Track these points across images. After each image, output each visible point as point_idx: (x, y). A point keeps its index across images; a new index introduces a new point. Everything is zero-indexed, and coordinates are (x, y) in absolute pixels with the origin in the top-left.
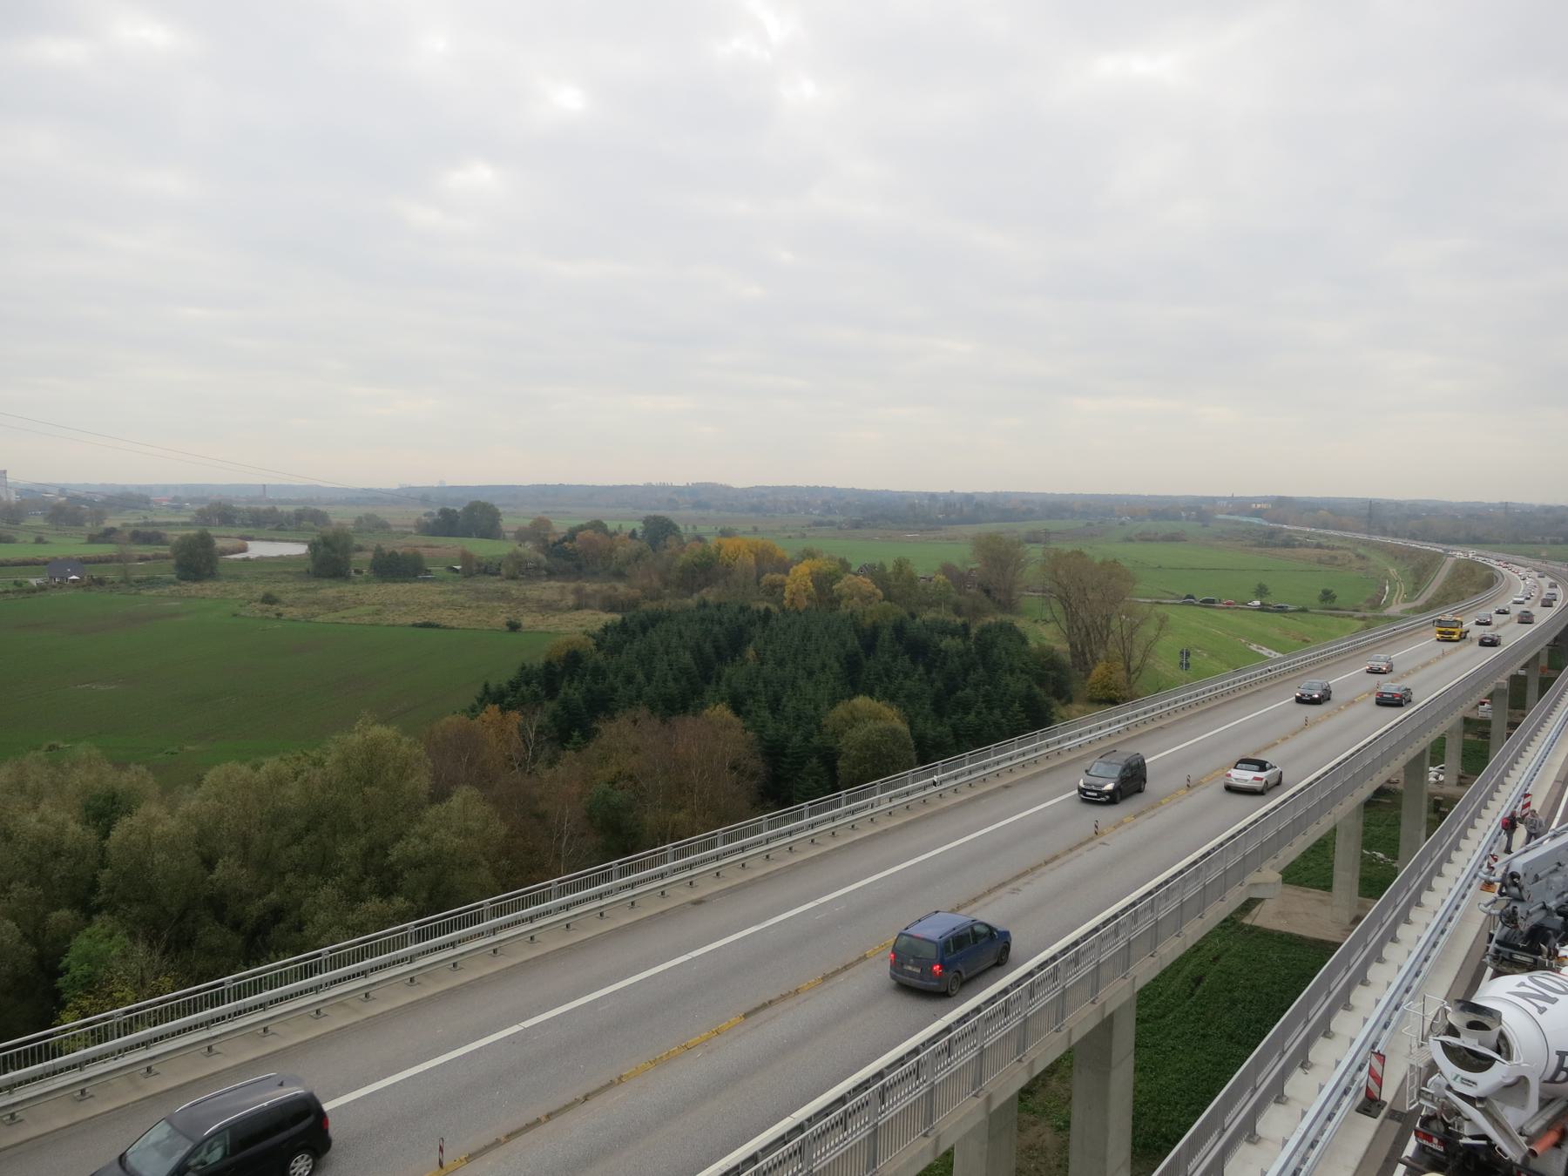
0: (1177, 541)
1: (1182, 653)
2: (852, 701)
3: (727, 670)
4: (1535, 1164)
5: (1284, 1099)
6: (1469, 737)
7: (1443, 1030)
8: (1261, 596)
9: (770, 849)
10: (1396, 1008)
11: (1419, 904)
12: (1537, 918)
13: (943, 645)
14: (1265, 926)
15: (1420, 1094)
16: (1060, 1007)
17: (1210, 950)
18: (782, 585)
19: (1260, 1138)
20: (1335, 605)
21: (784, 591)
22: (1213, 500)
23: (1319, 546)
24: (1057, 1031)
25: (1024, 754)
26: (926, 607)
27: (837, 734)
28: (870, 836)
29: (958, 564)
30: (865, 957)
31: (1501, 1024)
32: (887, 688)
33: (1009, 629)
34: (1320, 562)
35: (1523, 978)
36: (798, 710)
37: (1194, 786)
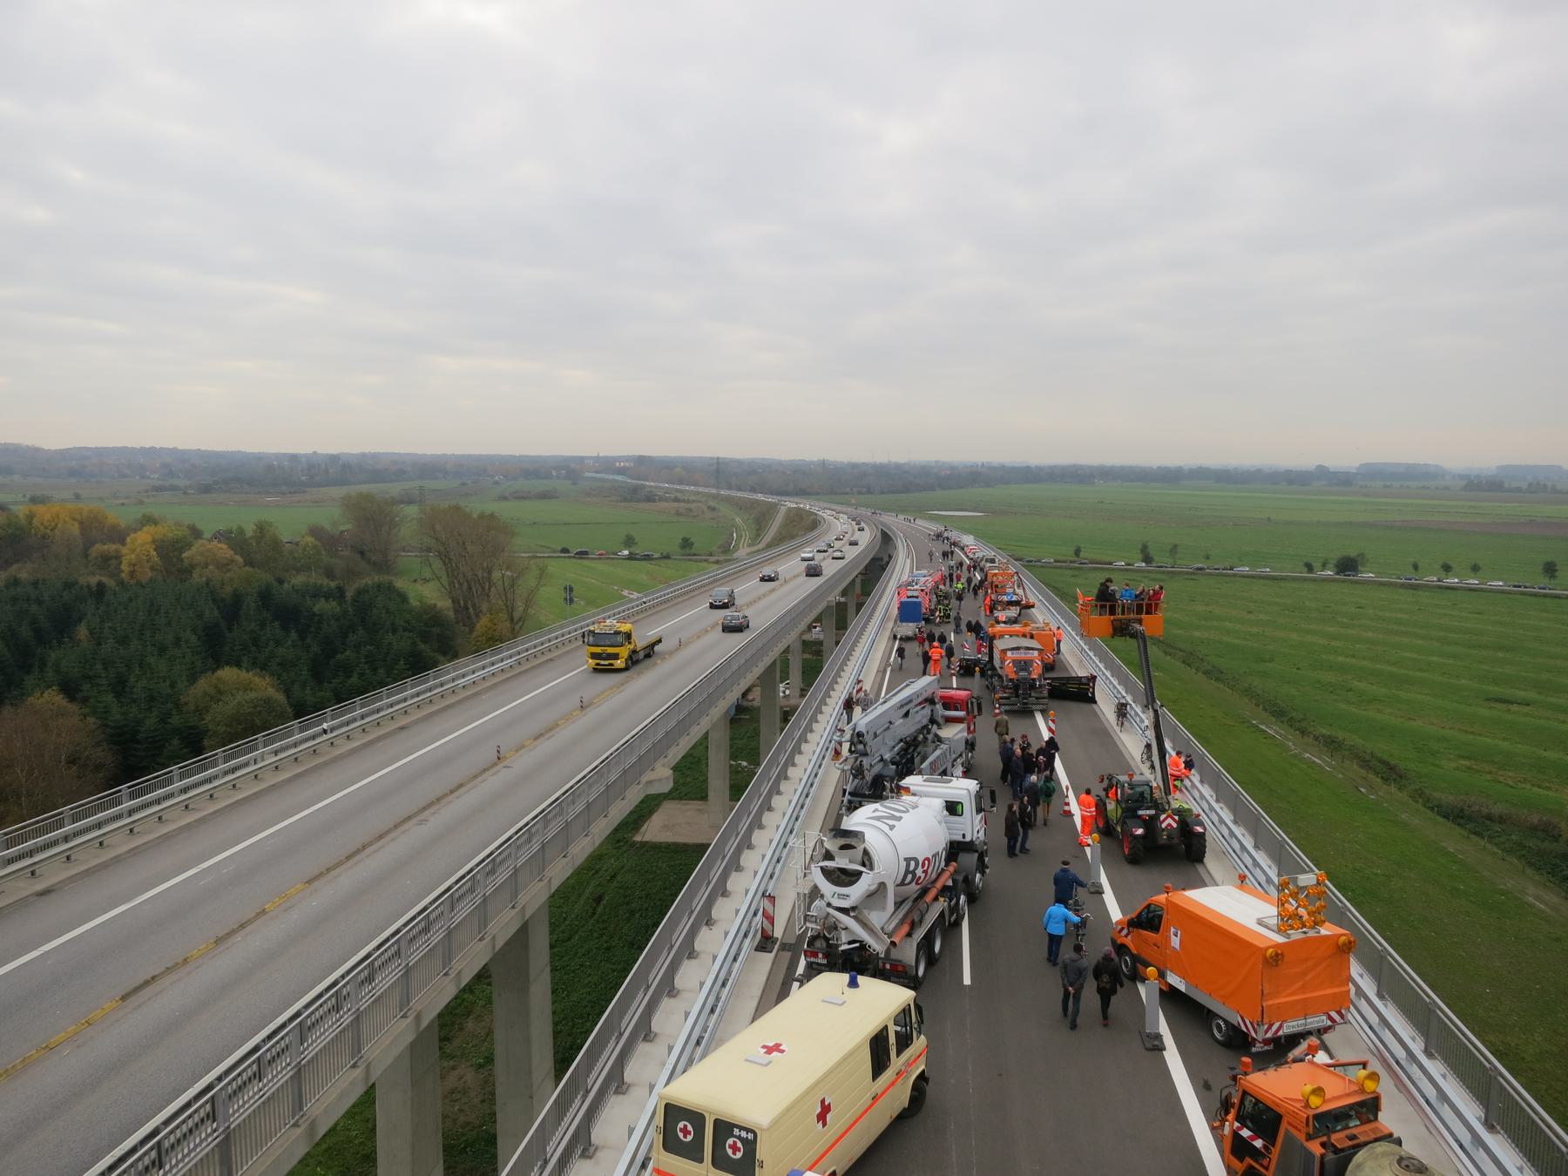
0: (550, 498)
1: (566, 588)
2: (216, 674)
3: (53, 655)
4: (895, 954)
5: (695, 954)
6: (807, 656)
7: (821, 857)
9: (135, 821)
10: (785, 846)
11: (786, 778)
12: (877, 769)
13: (316, 609)
14: (654, 840)
15: (806, 918)
16: (482, 914)
17: (607, 870)
18: (118, 557)
19: (678, 991)
20: (693, 551)
21: (121, 563)
22: (581, 460)
23: (676, 500)
24: (480, 940)
25: (418, 695)
26: (294, 572)
27: (200, 711)
28: (255, 794)
29: (327, 526)
30: (263, 912)
31: (864, 842)
32: (255, 658)
33: (390, 588)
34: (678, 514)
35: (877, 806)
36: (150, 689)
37: (587, 707)
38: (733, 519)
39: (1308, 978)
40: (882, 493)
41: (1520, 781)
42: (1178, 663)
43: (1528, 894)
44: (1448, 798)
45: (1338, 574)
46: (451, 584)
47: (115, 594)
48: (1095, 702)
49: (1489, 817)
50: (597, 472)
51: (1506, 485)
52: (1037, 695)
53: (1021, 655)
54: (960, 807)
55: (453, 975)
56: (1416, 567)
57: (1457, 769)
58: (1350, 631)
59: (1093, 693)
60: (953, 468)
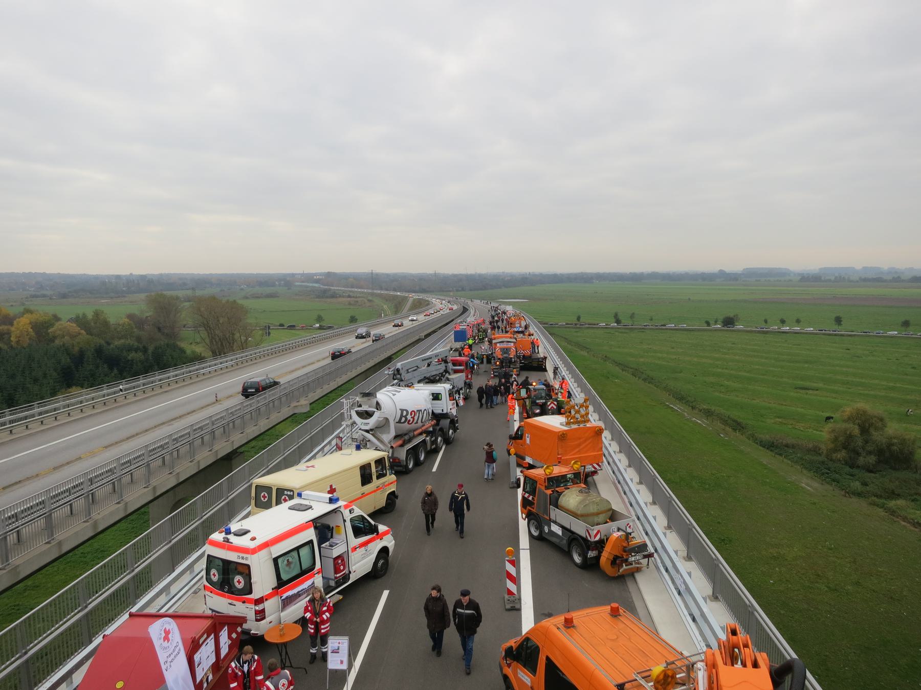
8: (320, 322)
13: (129, 358)
18: (9, 333)
21: (10, 336)
23: (349, 296)
24: (191, 462)
29: (137, 312)
30: (80, 458)
34: (350, 304)
38: (382, 306)
39: (581, 447)
40: (471, 290)
41: (807, 428)
42: (629, 375)
43: (802, 483)
44: (766, 437)
45: (723, 327)
46: (211, 342)
47: (7, 352)
48: (546, 371)
49: (787, 446)
50: (303, 282)
51: (823, 278)
52: (514, 367)
53: (505, 345)
54: (440, 396)
55: (174, 474)
56: (766, 321)
57: (775, 423)
58: (727, 356)
59: (545, 366)
60: (512, 276)
